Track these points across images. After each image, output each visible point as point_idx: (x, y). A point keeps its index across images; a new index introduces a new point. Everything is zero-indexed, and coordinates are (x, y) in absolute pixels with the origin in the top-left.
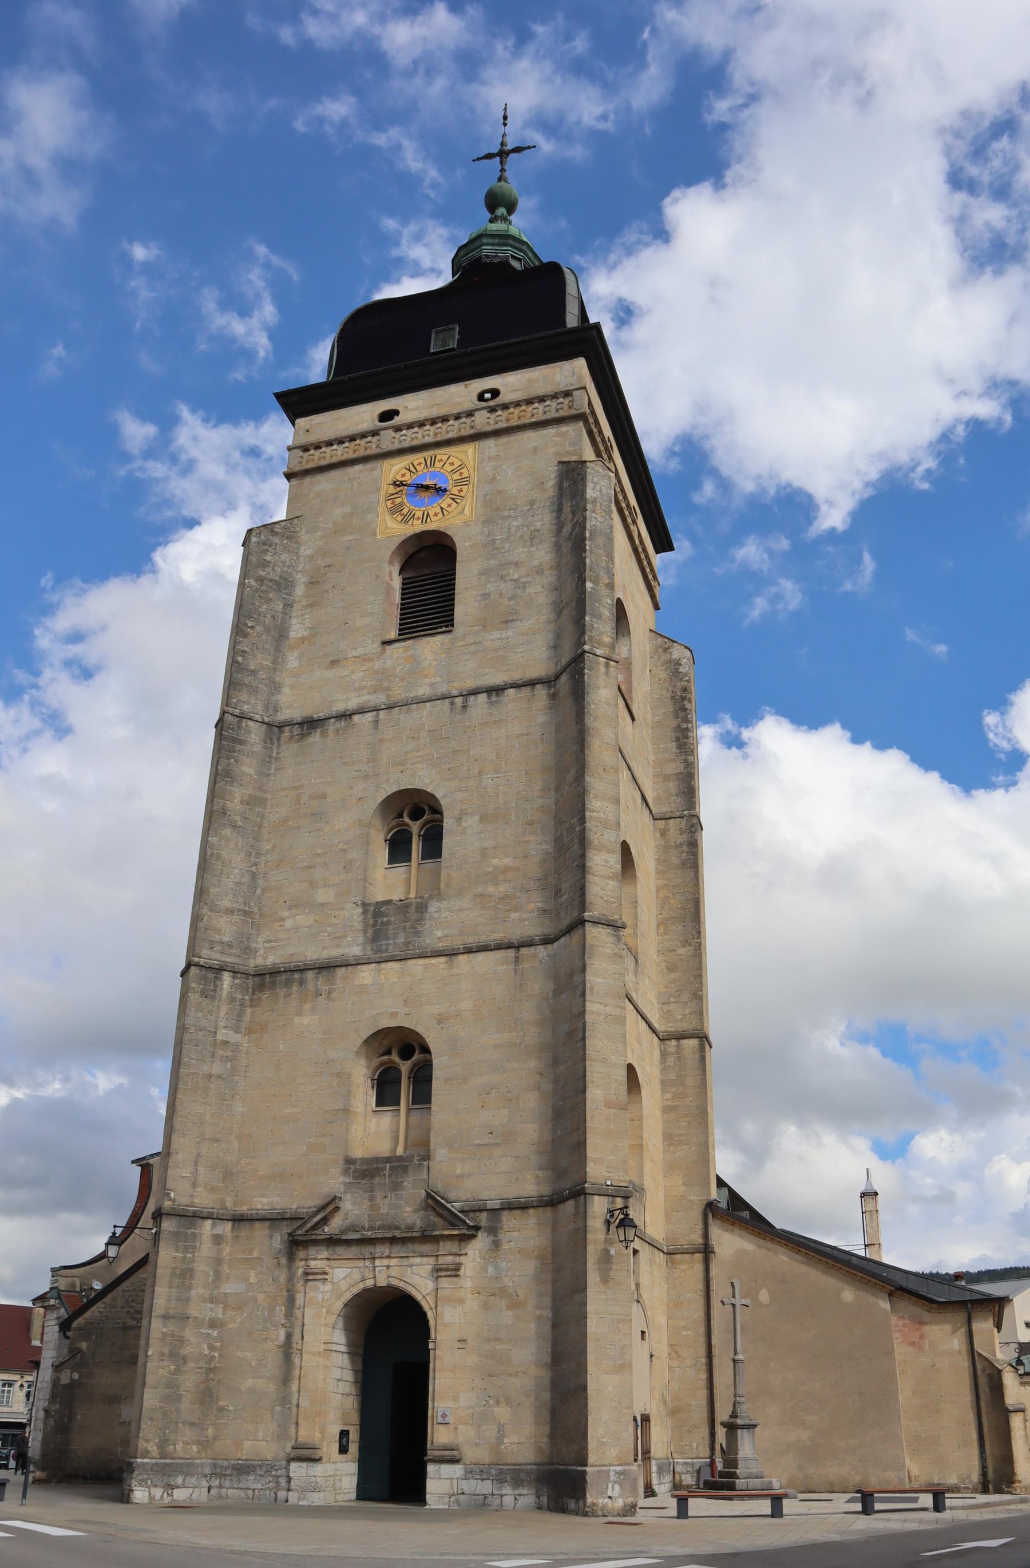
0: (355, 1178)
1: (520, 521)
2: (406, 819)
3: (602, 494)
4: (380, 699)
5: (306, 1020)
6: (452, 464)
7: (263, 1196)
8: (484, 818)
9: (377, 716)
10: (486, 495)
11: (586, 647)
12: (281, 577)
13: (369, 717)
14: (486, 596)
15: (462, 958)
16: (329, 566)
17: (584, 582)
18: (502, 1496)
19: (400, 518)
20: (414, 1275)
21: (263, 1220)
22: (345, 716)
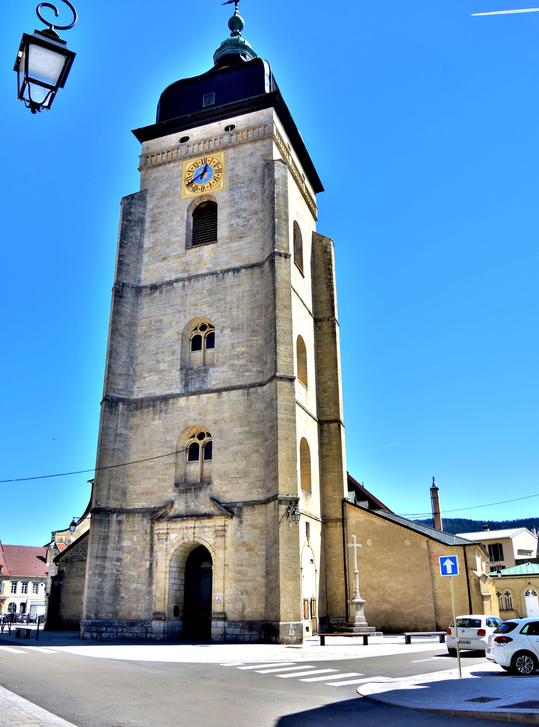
0: (179, 493)
1: (246, 189)
2: (199, 331)
3: (282, 176)
4: (186, 275)
5: (156, 422)
6: (214, 162)
7: (139, 502)
8: (233, 330)
9: (184, 283)
10: (230, 177)
11: (276, 250)
12: (138, 219)
13: (180, 284)
14: (231, 225)
15: (224, 393)
16: (160, 213)
17: (274, 219)
18: (244, 635)
19: (191, 189)
20: (208, 540)
21: (139, 513)
22: (170, 283)
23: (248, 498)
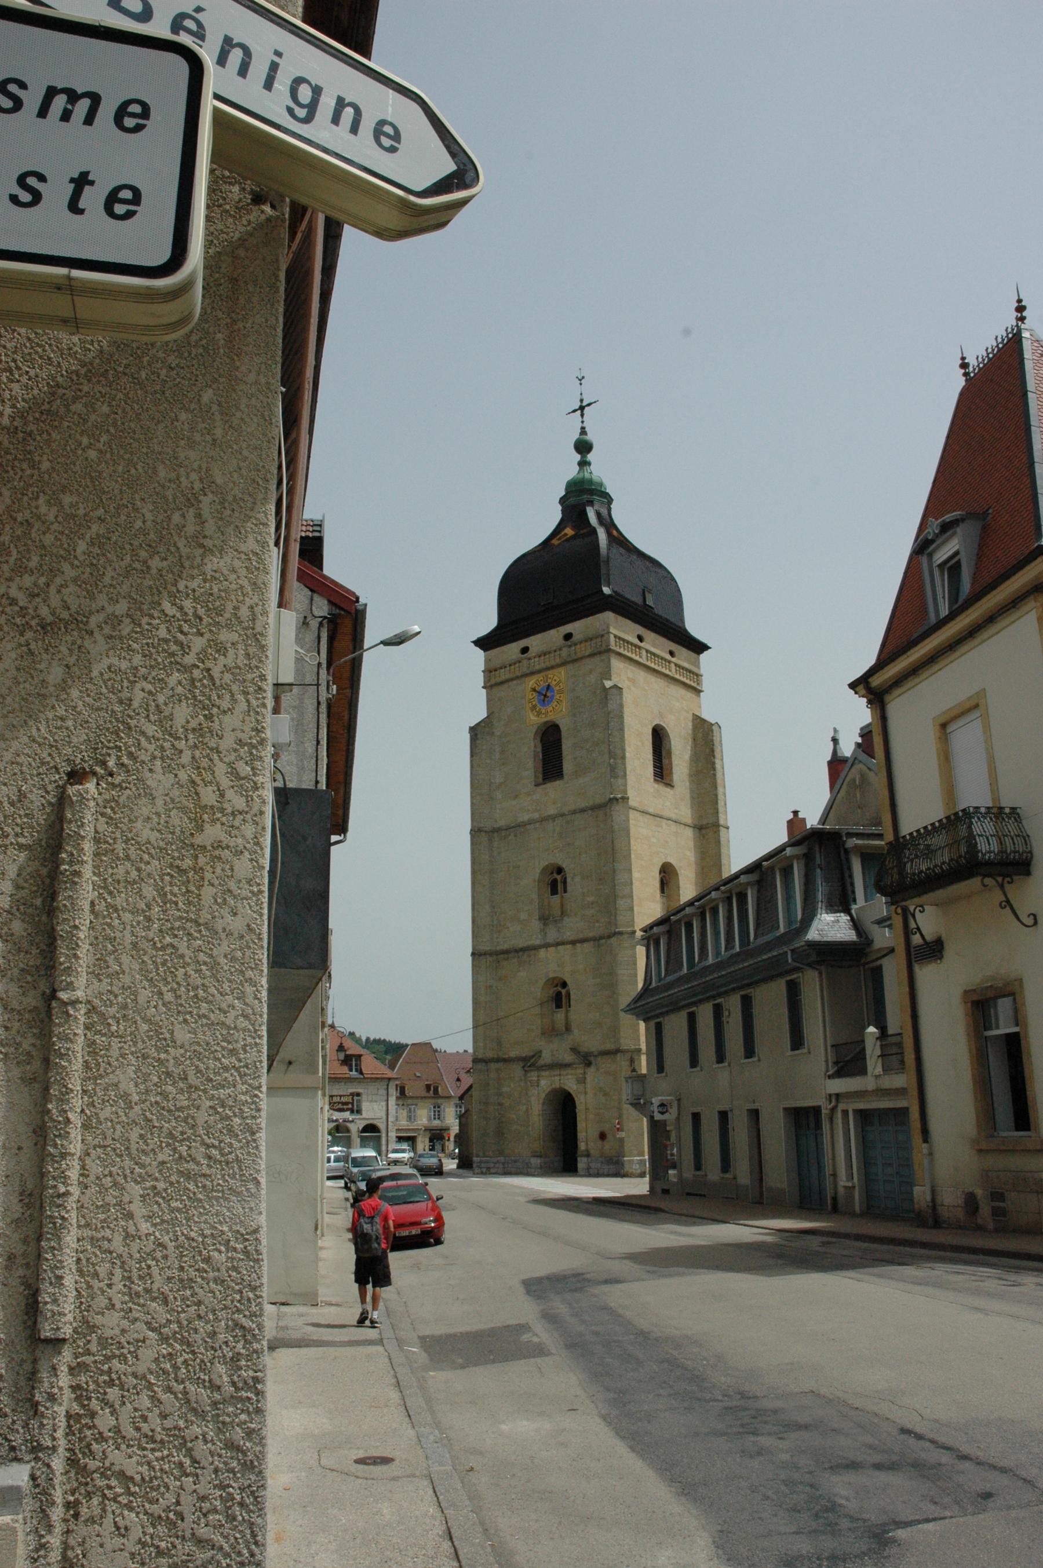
13: (532, 826)
14: (575, 758)
15: (578, 945)
20: (570, 1084)
23: (603, 1047)
